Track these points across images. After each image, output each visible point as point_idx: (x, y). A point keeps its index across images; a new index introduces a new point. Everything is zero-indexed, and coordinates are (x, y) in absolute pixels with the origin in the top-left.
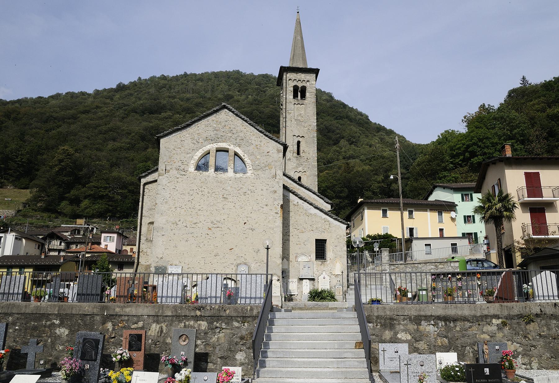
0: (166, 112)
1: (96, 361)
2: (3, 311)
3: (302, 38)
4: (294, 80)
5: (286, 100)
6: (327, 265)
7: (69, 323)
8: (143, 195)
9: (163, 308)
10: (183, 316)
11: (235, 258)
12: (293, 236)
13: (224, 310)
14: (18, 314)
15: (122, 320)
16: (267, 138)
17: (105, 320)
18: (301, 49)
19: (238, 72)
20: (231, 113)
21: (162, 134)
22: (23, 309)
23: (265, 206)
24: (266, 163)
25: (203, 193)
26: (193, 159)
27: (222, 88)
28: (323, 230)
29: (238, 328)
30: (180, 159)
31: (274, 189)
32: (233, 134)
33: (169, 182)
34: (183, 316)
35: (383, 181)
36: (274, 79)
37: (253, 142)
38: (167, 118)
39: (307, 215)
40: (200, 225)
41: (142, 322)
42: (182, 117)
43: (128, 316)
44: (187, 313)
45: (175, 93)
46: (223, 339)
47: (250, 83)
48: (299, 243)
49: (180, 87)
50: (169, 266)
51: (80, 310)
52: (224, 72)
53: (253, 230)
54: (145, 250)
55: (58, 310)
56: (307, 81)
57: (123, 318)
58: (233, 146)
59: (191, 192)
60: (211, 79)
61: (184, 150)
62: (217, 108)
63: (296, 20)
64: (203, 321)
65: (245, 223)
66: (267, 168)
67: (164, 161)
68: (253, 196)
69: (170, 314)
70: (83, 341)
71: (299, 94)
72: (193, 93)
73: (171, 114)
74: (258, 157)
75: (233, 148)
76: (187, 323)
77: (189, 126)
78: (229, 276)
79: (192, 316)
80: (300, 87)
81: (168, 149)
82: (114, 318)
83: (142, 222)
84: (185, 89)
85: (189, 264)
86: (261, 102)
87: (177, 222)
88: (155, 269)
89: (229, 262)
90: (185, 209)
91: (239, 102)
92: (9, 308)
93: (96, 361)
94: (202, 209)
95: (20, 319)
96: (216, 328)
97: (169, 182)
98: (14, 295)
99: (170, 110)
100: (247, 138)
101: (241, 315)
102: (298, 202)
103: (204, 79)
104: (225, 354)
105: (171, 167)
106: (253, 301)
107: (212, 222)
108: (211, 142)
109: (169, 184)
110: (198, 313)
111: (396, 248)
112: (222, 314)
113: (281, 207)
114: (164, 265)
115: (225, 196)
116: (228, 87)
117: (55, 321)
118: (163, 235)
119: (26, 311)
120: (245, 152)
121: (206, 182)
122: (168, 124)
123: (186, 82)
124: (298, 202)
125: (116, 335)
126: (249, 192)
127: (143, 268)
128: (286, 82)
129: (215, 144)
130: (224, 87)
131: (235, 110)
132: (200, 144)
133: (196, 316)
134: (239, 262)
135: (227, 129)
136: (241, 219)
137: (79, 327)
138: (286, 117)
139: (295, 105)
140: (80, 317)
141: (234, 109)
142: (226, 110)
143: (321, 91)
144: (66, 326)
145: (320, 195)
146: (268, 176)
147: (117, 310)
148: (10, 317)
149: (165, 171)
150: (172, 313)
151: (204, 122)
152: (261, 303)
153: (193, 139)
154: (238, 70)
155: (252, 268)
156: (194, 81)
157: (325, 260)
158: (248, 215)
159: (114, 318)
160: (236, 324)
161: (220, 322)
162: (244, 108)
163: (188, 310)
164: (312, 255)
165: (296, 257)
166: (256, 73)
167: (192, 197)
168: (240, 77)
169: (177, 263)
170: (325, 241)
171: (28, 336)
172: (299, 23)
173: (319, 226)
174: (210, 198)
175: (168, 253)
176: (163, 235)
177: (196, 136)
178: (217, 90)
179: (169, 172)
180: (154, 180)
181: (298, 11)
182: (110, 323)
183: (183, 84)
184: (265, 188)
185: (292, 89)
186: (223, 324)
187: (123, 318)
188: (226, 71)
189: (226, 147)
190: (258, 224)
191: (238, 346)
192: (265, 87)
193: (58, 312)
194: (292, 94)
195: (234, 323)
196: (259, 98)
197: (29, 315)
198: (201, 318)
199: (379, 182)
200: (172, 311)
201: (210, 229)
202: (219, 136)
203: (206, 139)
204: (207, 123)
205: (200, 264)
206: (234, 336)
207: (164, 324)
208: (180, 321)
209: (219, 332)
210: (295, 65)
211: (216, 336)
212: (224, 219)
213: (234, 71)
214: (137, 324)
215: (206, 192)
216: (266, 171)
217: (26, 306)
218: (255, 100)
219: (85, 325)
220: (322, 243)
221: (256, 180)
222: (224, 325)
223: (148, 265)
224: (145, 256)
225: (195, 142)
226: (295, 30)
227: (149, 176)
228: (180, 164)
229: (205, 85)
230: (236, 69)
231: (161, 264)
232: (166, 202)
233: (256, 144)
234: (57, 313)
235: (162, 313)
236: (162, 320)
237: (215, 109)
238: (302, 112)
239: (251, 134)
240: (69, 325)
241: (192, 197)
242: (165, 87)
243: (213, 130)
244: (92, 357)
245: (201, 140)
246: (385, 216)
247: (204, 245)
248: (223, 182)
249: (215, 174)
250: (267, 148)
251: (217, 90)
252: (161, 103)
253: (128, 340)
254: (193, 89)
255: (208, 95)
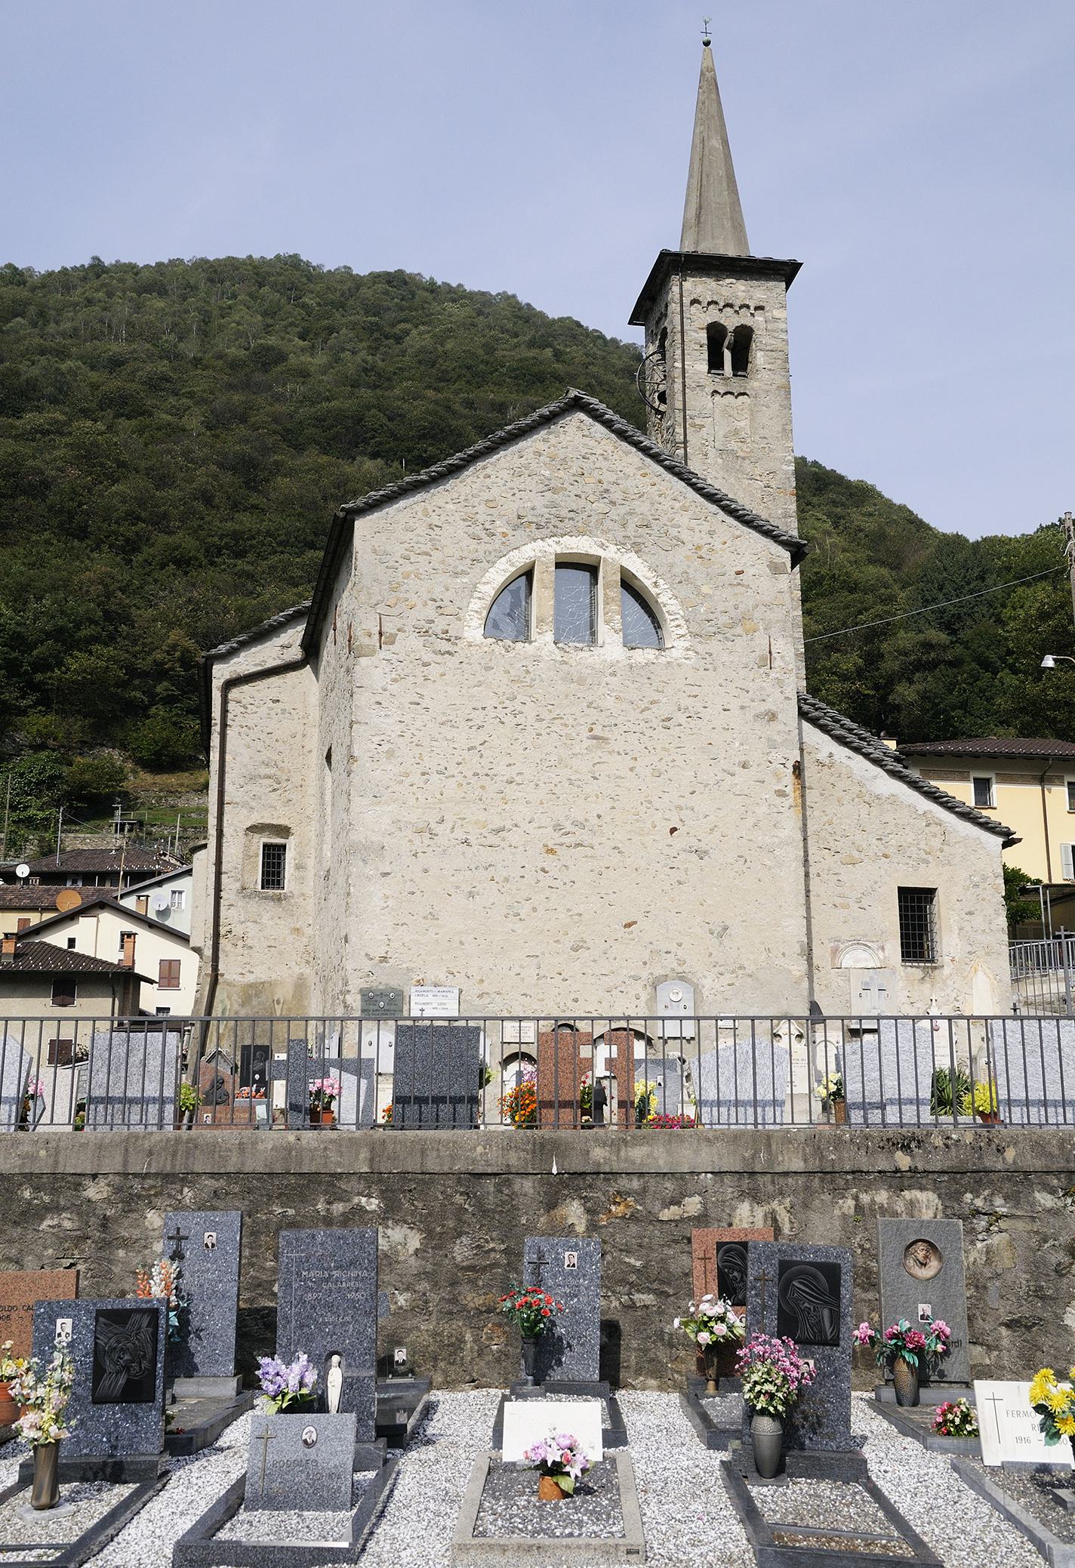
0: (39, 409)
1: (838, 1345)
2: (154, 1164)
3: (725, 143)
4: (709, 303)
5: (684, 378)
6: (944, 982)
7: (420, 1205)
8: (224, 725)
9: (770, 1145)
10: (847, 1173)
11: (647, 954)
12: (818, 875)
13: (994, 1147)
14: (213, 1175)
15: (618, 1192)
16: (730, 520)
17: (557, 1192)
18: (725, 185)
19: (293, 263)
20: (598, 427)
21: (360, 501)
22: (234, 1159)
23: (738, 770)
24: (733, 613)
25: (520, 719)
26: (476, 595)
27: (238, 324)
28: (924, 856)
29: (1053, 1212)
30: (430, 596)
31: (768, 706)
32: (613, 503)
33: (395, 680)
34: (847, 1173)
35: (860, 673)
36: (427, 290)
37: (683, 537)
38: (45, 433)
39: (866, 799)
40: (514, 837)
41: (697, 1199)
42: (103, 428)
43: (642, 1174)
44: (863, 1162)
45: (63, 335)
46: (1007, 1254)
47: (342, 306)
48: (841, 900)
49: (80, 316)
50: (414, 989)
51: (453, 1158)
52: (243, 262)
53: (701, 854)
54: (238, 930)
55: (372, 1160)
56: (757, 308)
57: (624, 1183)
58: (613, 548)
59: (478, 717)
60: (194, 288)
61: (443, 562)
62: (553, 406)
63: (702, 74)
64: (922, 1189)
65: (673, 830)
66: (739, 630)
67: (373, 601)
68: (694, 731)
69: (798, 1165)
70: (781, 1275)
71: (727, 355)
72: (131, 339)
73: (63, 418)
74: (705, 589)
75: (617, 556)
76: (865, 1198)
77: (454, 471)
78: (639, 1026)
79: (880, 1172)
80: (731, 328)
81: (385, 558)
82: (590, 1186)
83: (225, 824)
84: (102, 321)
85: (482, 981)
86: (389, 379)
87: (433, 825)
88: (362, 1000)
89: (625, 972)
90: (460, 778)
91: (309, 375)
92: (174, 1155)
93: (838, 1345)
94: (518, 779)
95: (227, 1194)
96: (974, 1216)
97: (395, 680)
98: (759, 1110)
99: (54, 401)
100: (664, 520)
101: (1061, 1164)
102: (831, 755)
103: (169, 287)
104: (1025, 1311)
105: (398, 622)
106: (875, 1116)
107: (558, 827)
108: (537, 534)
109: (396, 685)
110: (903, 1161)
111: (1040, 918)
112: (990, 1161)
113: (794, 772)
114: (394, 983)
115: (598, 731)
116: (260, 318)
117: (364, 1200)
118: (385, 874)
119: (243, 1164)
120: (661, 571)
121: (528, 679)
122: (57, 453)
123: (101, 295)
124: (831, 755)
125: (608, 1248)
126: (681, 718)
127: (235, 997)
128: (682, 311)
129: (550, 541)
130: (247, 317)
131: (616, 417)
132: (498, 540)
133: (897, 1171)
134: (659, 971)
135: (589, 486)
136: (660, 814)
137: (460, 1220)
138: (685, 442)
139: (717, 397)
140: (459, 1181)
141: (611, 412)
142: (582, 416)
143: (602, 337)
144: (409, 1219)
145: (854, 726)
146: (744, 660)
147: (598, 1154)
148: (186, 1190)
149: (377, 636)
150: (805, 1161)
151: (505, 459)
152: (1047, 1124)
153: (470, 520)
154: (296, 256)
155: (706, 993)
156: (134, 295)
157: (932, 961)
158: (682, 802)
159: (590, 1186)
160: (1045, 1200)
161: (986, 1193)
162: (328, 399)
163: (863, 1152)
164: (888, 946)
165: (835, 952)
166: (361, 269)
167: (482, 736)
168: (304, 280)
169: (442, 977)
170: (928, 894)
171: (266, 1260)
172: (709, 83)
173: (910, 840)
174: (545, 737)
175: (407, 939)
176: (385, 874)
177: (481, 508)
178: (221, 328)
179: (393, 643)
180: (259, 668)
181: (706, 39)
182: (576, 1204)
183: (89, 302)
184: (734, 705)
185: (703, 337)
186: (999, 1201)
187: (624, 1183)
188: (250, 257)
189: (592, 552)
190: (717, 834)
191: (1065, 1280)
192: (400, 322)
193: (371, 1167)
194: (706, 356)
195: (1037, 1195)
196: (380, 363)
197: (258, 1180)
198: (914, 1178)
199: (845, 678)
200: (805, 1155)
201: (551, 851)
202: (564, 513)
203: (520, 522)
204: (517, 462)
205: (523, 980)
206: (1046, 1242)
207: (781, 1203)
208: (838, 1193)
209: (988, 1230)
210: (706, 248)
211: (979, 1245)
212: (599, 816)
213: (278, 257)
214: (678, 1203)
215: (532, 716)
216: (738, 640)
217: (241, 1147)
218: (365, 370)
219: (483, 1212)
220: (920, 900)
221: (702, 672)
222: (1000, 1206)
223: (251, 986)
224: (239, 950)
225: (478, 530)
226: (699, 110)
227: (243, 654)
228: (430, 612)
229: (177, 307)
230: (287, 250)
231: (383, 979)
232: (390, 754)
233: (697, 541)
234: (366, 1169)
235: (771, 1161)
236: (770, 1188)
237: (545, 411)
238: (742, 424)
239: (677, 505)
240: (421, 1215)
241: (482, 736)
242: (22, 315)
243: (541, 487)
244: (822, 1330)
245: (500, 527)
246: (985, 803)
247: (535, 910)
248: (589, 681)
249: (557, 651)
250: (734, 556)
251: (221, 328)
252: (18, 374)
253: (713, 1266)
254: (129, 324)
255: (190, 348)
